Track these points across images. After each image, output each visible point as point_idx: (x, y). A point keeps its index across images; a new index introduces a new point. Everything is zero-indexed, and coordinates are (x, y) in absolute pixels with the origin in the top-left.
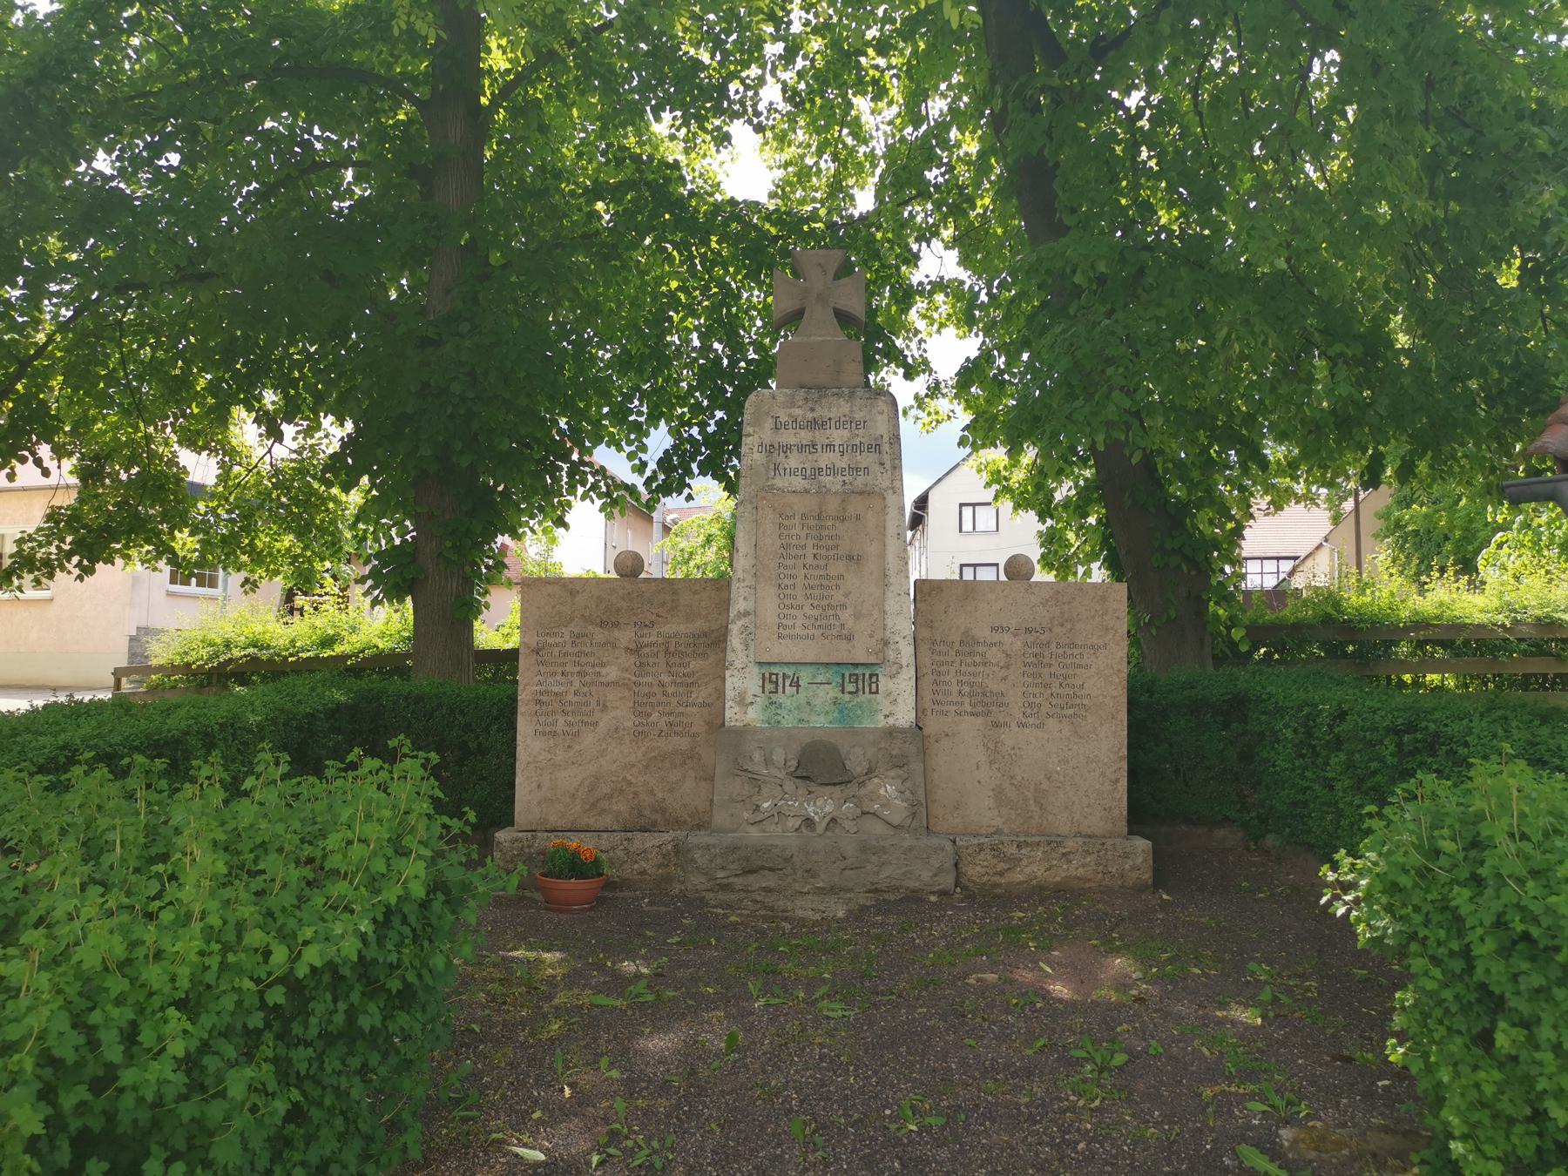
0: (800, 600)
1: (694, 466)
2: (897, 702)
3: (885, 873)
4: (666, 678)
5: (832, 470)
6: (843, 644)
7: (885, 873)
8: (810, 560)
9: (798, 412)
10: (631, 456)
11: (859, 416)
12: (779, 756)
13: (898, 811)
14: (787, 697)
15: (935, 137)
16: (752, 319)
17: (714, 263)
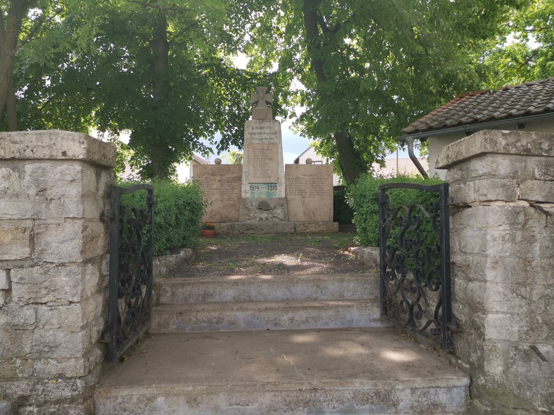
0: (259, 169)
1: (230, 142)
2: (280, 192)
3: (279, 229)
4: (227, 188)
5: (266, 139)
6: (269, 179)
7: (279, 229)
8: (261, 159)
9: (257, 125)
10: (209, 140)
11: (272, 126)
12: (254, 204)
13: (281, 216)
14: (256, 191)
15: (295, 48)
16: (243, 101)
17: (233, 87)
